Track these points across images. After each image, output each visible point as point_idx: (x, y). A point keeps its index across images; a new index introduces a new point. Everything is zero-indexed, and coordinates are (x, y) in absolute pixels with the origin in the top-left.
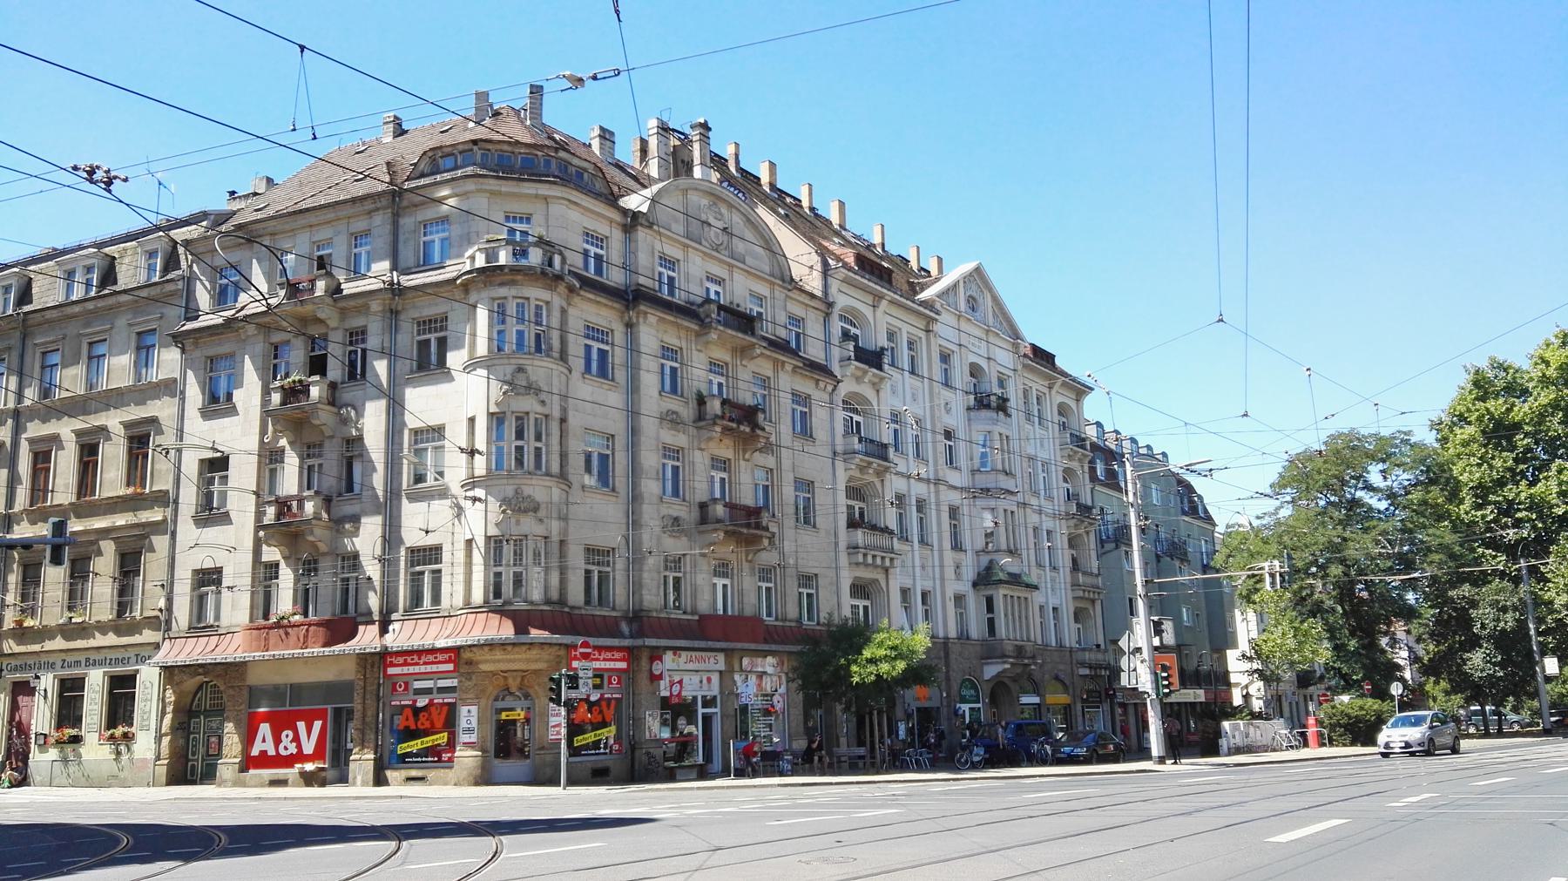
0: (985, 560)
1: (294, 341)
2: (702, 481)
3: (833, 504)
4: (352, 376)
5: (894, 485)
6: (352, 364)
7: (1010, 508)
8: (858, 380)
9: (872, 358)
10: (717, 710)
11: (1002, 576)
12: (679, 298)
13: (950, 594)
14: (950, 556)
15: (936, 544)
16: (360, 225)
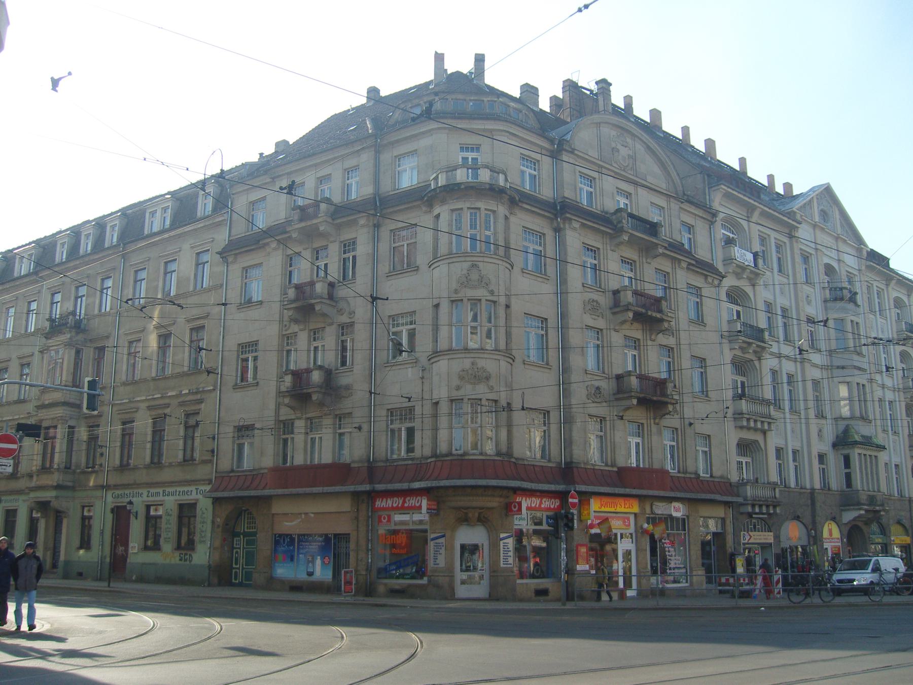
0: (842, 425)
5: (769, 363)
11: (857, 438)
12: (596, 208)
13: (815, 453)
16: (350, 162)
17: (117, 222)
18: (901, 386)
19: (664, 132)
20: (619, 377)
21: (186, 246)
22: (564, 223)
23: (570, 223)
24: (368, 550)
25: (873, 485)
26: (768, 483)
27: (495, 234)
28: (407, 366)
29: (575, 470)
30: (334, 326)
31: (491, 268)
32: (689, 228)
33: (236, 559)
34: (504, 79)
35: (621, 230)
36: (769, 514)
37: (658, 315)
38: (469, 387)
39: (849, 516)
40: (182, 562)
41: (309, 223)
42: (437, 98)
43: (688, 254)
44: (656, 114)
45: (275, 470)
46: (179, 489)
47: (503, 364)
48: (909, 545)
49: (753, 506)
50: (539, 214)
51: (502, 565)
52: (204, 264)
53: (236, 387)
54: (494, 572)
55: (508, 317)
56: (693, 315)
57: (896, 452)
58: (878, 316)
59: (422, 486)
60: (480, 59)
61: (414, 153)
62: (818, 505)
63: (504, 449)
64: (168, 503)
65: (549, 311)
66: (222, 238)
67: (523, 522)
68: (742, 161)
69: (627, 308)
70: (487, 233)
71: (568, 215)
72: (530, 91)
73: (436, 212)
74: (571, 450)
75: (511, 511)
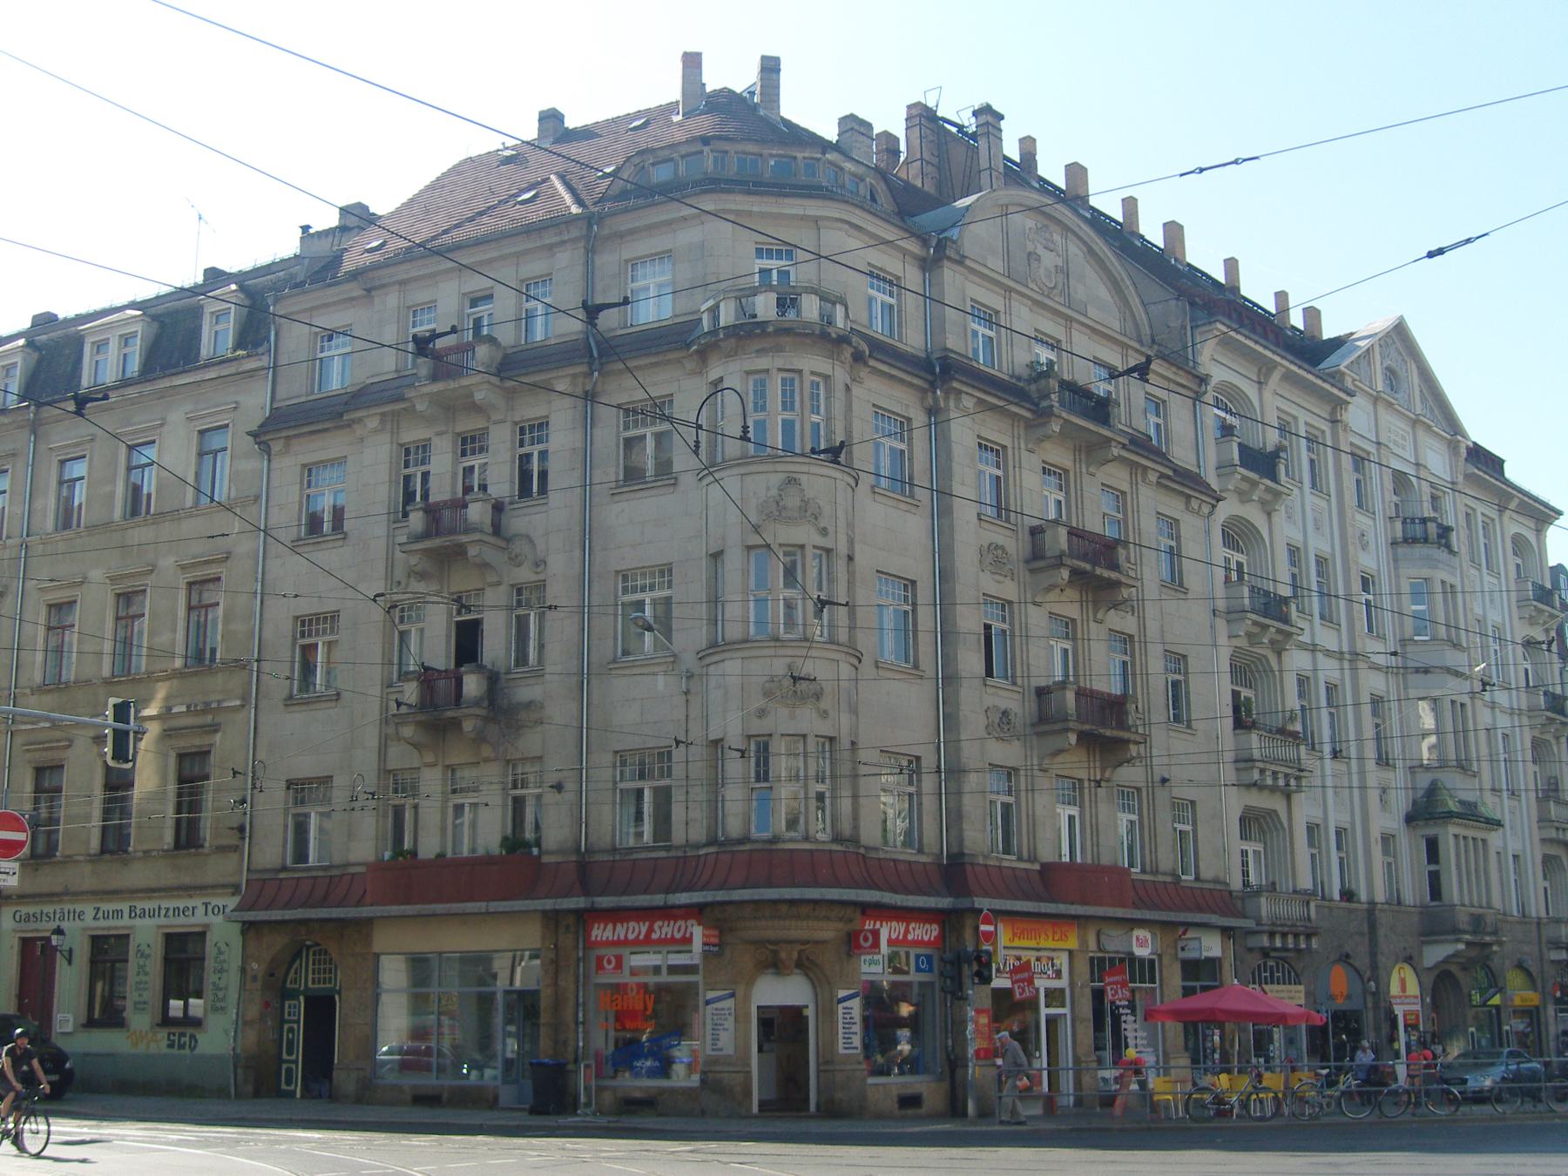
0: (1424, 780)
1: (436, 441)
2: (1046, 660)
3: (1213, 692)
4: (525, 491)
5: (1297, 660)
6: (525, 476)
7: (1459, 699)
8: (1243, 497)
9: (1263, 463)
10: (1065, 1011)
11: (1453, 806)
12: (1001, 371)
13: (1375, 834)
14: (1374, 775)
15: (1353, 754)
16: (534, 267)
17: (18, 359)
18: (1524, 706)
19: (1041, 179)
20: (1041, 692)
21: (176, 416)
22: (946, 399)
23: (958, 400)
24: (577, 1023)
25: (1479, 895)
26: (1295, 892)
27: (828, 419)
28: (656, 669)
29: (968, 868)
30: (503, 588)
31: (820, 481)
32: (1157, 405)
33: (290, 1043)
34: (812, 107)
35: (1047, 414)
36: (1298, 951)
37: (1114, 575)
38: (783, 712)
39: (1434, 954)
40: (175, 1051)
41: (452, 385)
42: (706, 149)
43: (1160, 455)
44: (1076, 172)
45: (378, 867)
46: (165, 904)
47: (845, 670)
48: (1537, 1008)
49: (1272, 935)
50: (902, 381)
51: (841, 1051)
52: (215, 453)
53: (289, 701)
54: (827, 1063)
55: (851, 574)
56: (1166, 575)
57: (1518, 835)
58: (1485, 571)
59: (695, 900)
60: (770, 67)
61: (665, 255)
62: (1381, 932)
63: (846, 828)
64: (146, 930)
65: (919, 568)
66: (256, 402)
67: (873, 968)
68: (1231, 265)
69: (1059, 562)
70: (815, 418)
71: (955, 384)
72: (853, 126)
73: (713, 375)
74: (961, 831)
75: (859, 947)
